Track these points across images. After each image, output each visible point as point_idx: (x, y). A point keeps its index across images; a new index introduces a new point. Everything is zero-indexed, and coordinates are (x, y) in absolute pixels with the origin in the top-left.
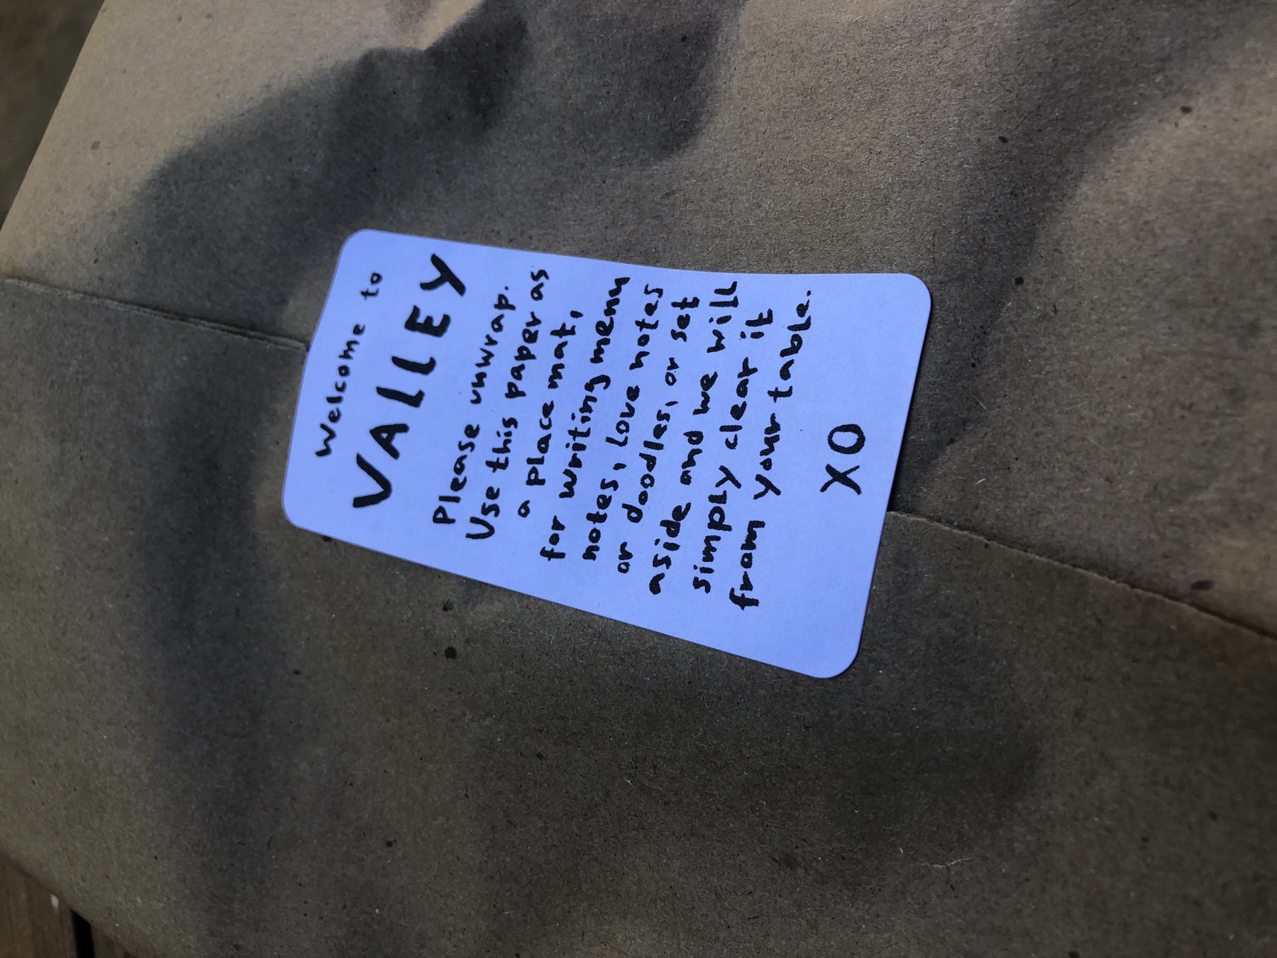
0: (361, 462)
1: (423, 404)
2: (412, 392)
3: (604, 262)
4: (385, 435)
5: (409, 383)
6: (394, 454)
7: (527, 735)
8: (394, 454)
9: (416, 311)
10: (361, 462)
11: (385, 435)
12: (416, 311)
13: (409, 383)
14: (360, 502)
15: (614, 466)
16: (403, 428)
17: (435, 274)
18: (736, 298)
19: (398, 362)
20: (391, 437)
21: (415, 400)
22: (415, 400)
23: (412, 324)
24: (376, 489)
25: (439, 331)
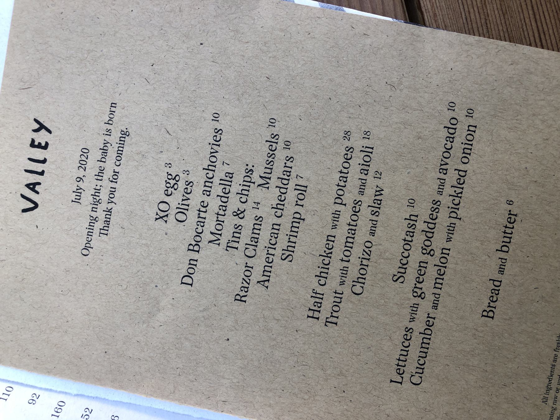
0: (23, 196)
1: (45, 174)
2: (40, 171)
3: (5, 39)
4: (32, 186)
5: (39, 167)
6: (37, 193)
7: (374, 105)
8: (37, 193)
9: (33, 141)
10: (23, 196)
11: (32, 186)
12: (33, 141)
13: (39, 167)
14: (24, 211)
15: (26, 184)
16: (39, 184)
17: (37, 126)
18: (320, 310)
19: (30, 159)
20: (34, 187)
21: (42, 173)
22: (42, 173)
23: (33, 145)
24: (32, 205)
25: (46, 147)
